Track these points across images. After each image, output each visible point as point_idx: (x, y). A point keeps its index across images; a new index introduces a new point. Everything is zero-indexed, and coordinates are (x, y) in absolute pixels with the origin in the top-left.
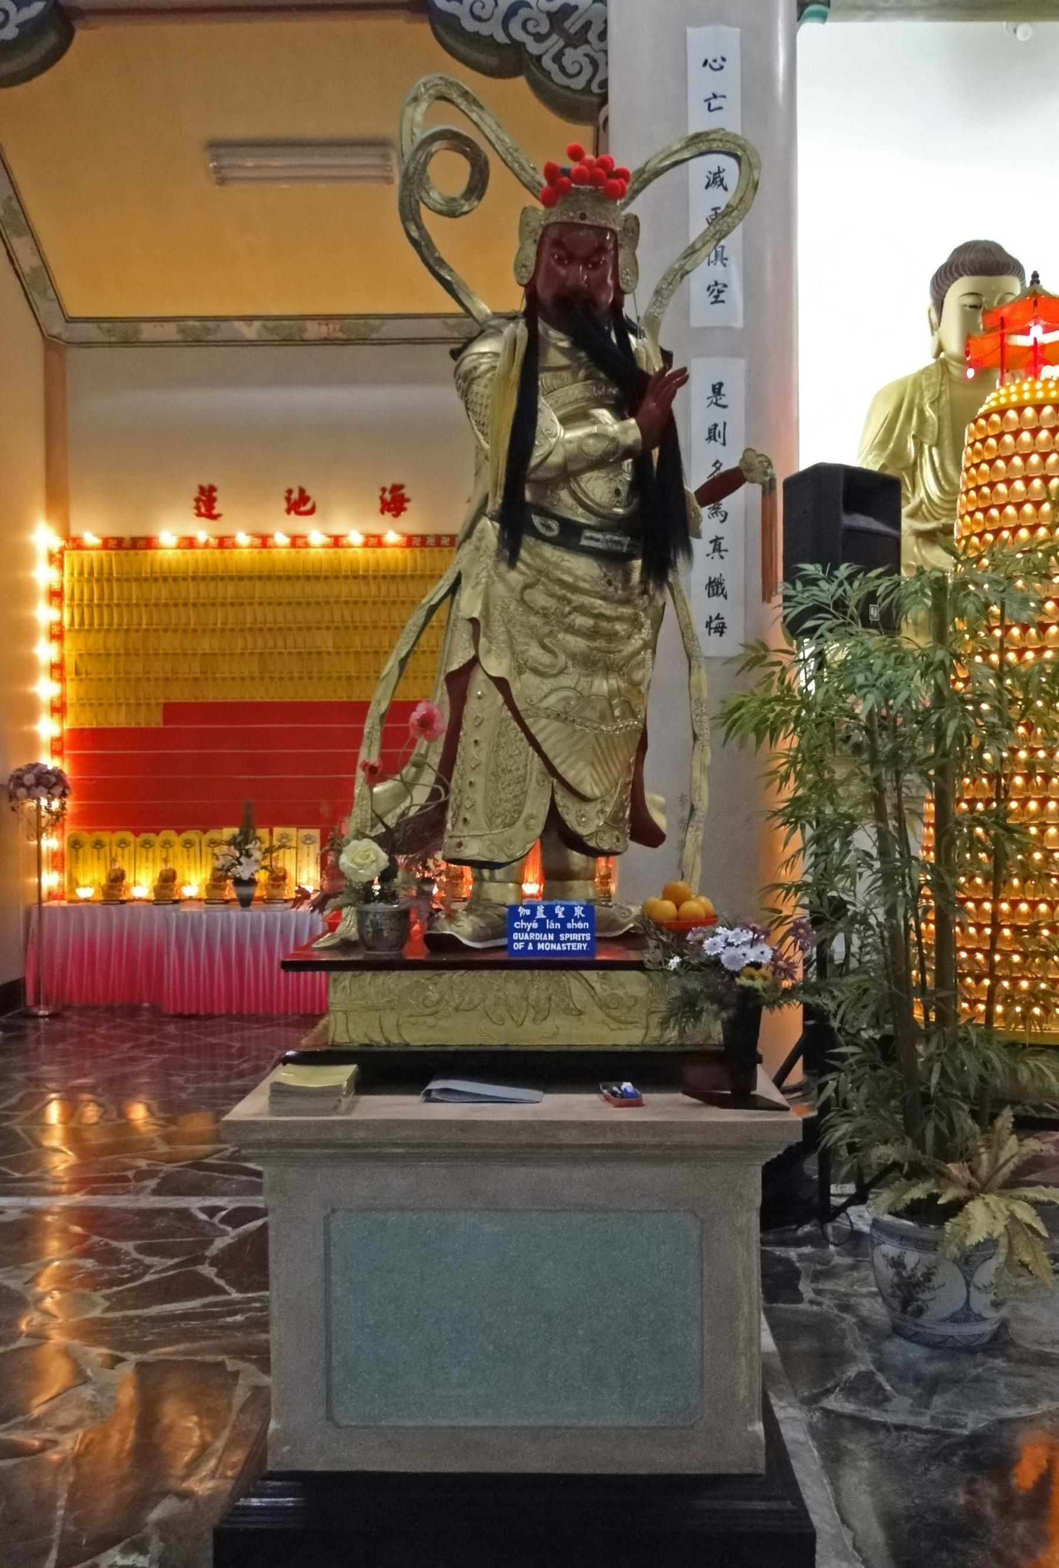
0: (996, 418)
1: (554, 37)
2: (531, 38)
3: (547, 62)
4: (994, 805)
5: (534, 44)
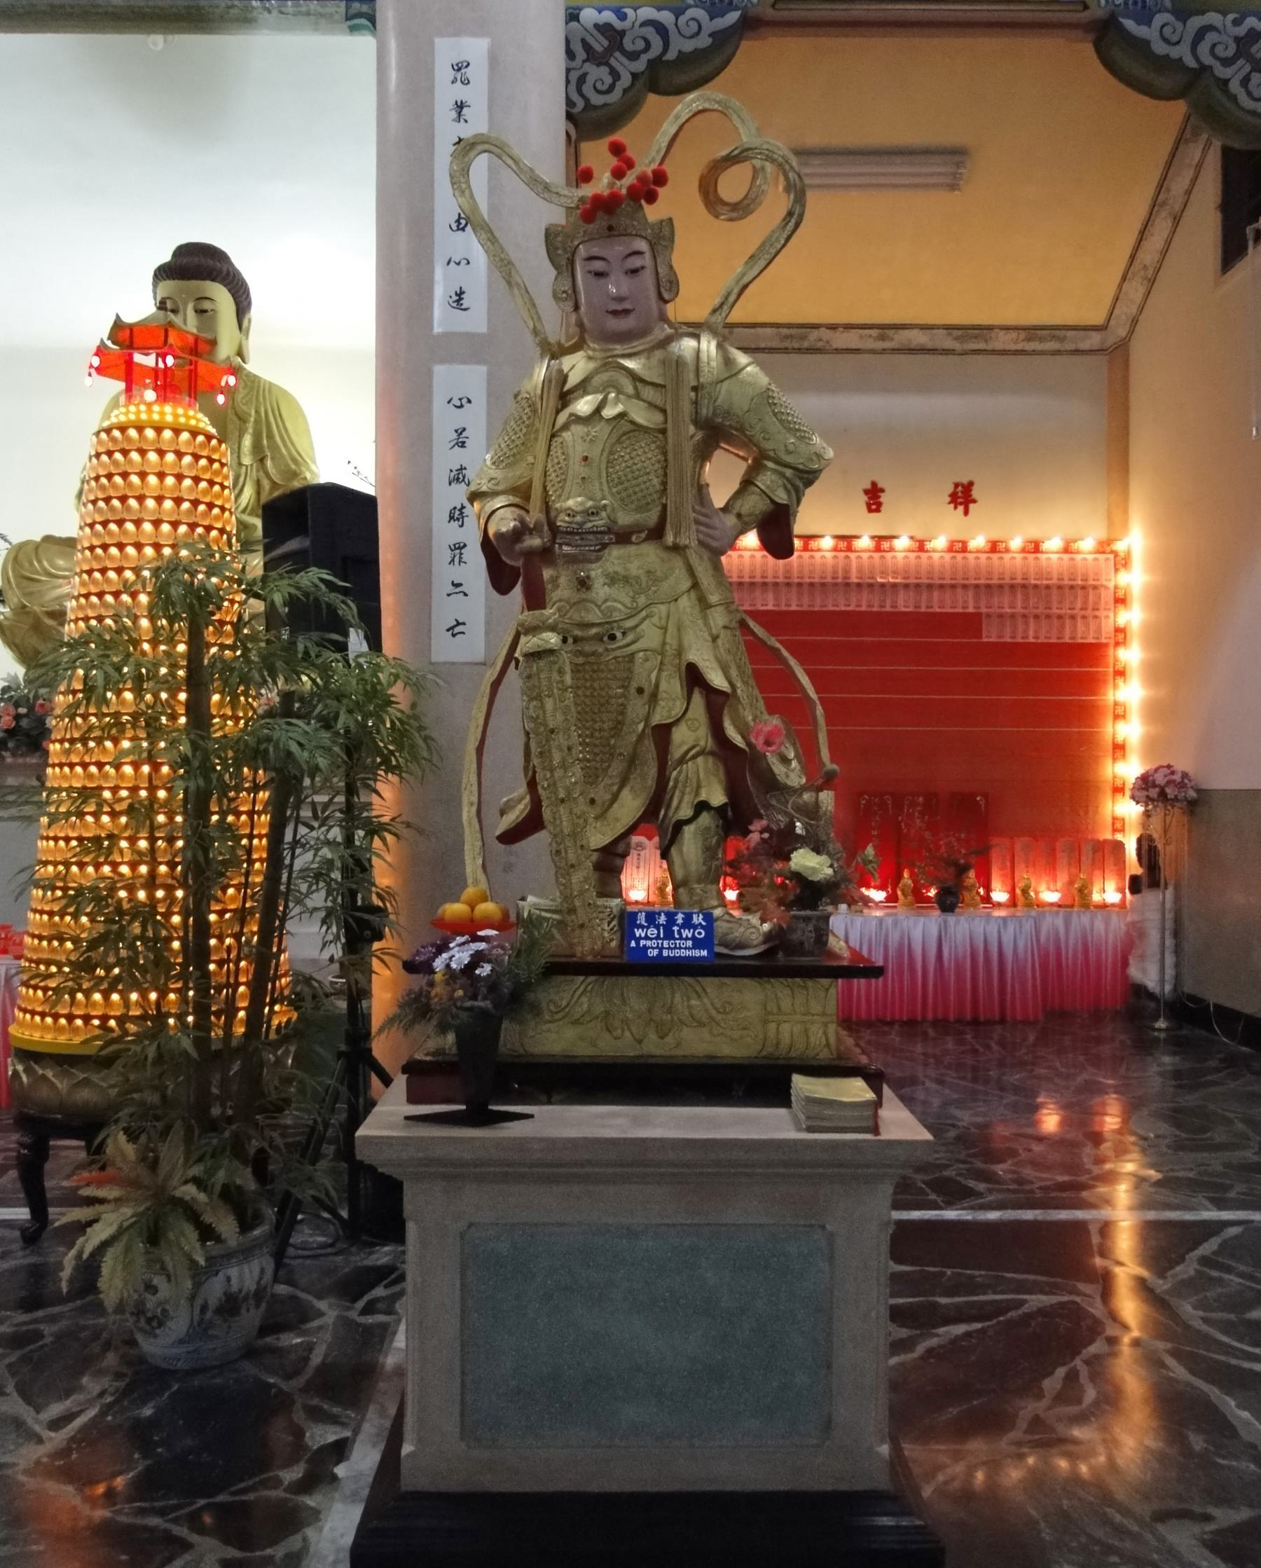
0: (116, 433)
1: (1241, 62)
2: (1218, 64)
3: (1235, 86)
4: (805, 860)
5: (1221, 68)
